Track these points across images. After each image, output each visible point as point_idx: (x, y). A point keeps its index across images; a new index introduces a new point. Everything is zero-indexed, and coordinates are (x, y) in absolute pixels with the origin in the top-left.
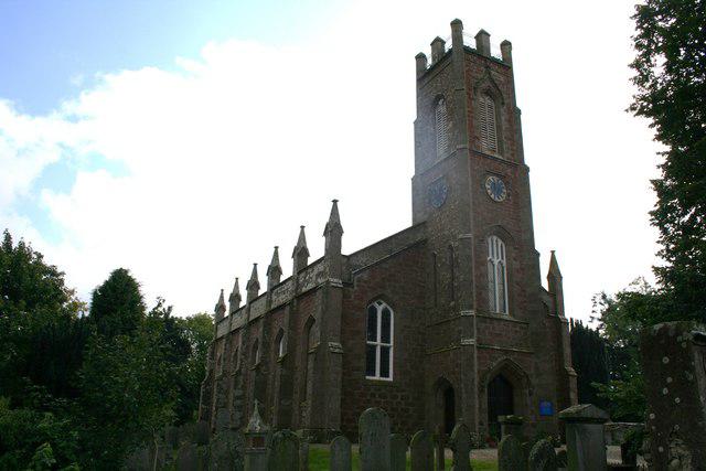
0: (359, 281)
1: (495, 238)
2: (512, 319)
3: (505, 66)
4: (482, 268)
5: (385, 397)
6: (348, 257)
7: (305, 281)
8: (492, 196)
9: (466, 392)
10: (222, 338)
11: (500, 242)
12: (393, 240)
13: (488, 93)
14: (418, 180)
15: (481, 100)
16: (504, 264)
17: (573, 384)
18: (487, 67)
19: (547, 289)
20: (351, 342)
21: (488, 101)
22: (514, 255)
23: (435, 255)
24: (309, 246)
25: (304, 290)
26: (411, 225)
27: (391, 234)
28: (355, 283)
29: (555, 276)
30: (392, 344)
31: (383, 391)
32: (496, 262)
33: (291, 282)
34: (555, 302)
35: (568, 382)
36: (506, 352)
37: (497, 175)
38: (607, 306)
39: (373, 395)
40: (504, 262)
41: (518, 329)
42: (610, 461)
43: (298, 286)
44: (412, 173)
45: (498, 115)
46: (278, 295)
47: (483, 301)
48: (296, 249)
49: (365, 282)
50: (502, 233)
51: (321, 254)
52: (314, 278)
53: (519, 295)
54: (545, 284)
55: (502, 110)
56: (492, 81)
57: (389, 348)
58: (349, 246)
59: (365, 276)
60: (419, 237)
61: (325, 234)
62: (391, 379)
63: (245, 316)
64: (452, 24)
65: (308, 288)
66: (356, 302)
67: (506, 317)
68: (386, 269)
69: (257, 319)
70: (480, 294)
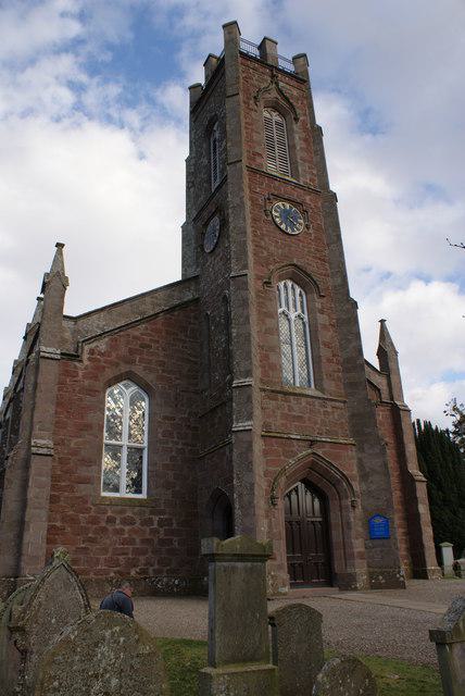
0: (92, 352)
1: (290, 283)
2: (320, 394)
3: (301, 79)
4: (268, 321)
5: (132, 522)
6: (75, 319)
8: (283, 227)
9: (242, 507)
11: (298, 290)
12: (148, 299)
13: (275, 107)
14: (190, 227)
15: (266, 114)
16: (306, 320)
17: (422, 491)
18: (273, 76)
19: (377, 367)
20: (75, 440)
21: (276, 117)
22: (318, 306)
26: (179, 278)
27: (145, 291)
28: (85, 356)
29: (386, 351)
30: (146, 444)
31: (129, 514)
32: (293, 316)
34: (389, 384)
35: (414, 490)
36: (312, 443)
37: (288, 200)
38: (458, 417)
39: (111, 520)
42: (204, 542)
44: (183, 219)
45: (290, 132)
47: (272, 368)
49: (102, 354)
50: (301, 277)
53: (329, 361)
54: (370, 354)
55: (295, 127)
56: (280, 91)
58: (74, 305)
59: (102, 345)
60: (189, 296)
62: (143, 496)
66: (87, 382)
67: (309, 392)
68: (135, 338)
70: (267, 356)
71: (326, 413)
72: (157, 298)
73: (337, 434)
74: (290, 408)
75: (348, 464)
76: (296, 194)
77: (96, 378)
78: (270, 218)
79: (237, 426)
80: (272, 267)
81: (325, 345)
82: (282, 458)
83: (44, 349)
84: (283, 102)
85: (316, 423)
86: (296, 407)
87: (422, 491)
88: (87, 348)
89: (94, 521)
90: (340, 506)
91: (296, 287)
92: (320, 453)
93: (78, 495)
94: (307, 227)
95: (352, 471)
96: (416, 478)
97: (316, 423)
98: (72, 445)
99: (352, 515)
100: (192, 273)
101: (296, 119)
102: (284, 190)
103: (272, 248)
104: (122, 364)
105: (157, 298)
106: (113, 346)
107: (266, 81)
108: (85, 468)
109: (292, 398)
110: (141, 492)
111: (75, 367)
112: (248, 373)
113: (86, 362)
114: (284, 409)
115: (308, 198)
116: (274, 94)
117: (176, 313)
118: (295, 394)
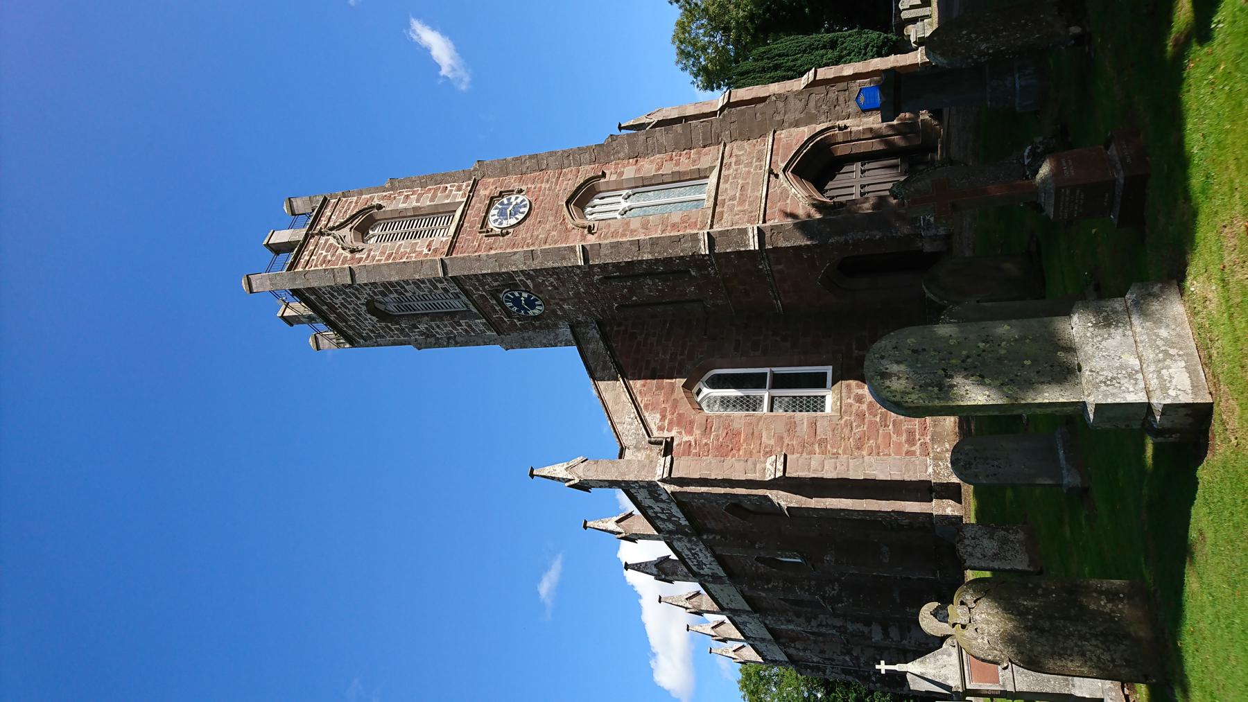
1: (588, 210)
7: (669, 520)
10: (786, 653)
11: (596, 201)
14: (508, 338)
17: (825, 73)
18: (321, 233)
23: (621, 307)
24: (653, 557)
25: (684, 522)
26: (575, 348)
28: (666, 434)
30: (767, 370)
32: (625, 205)
33: (676, 544)
37: (487, 212)
40: (624, 193)
41: (733, 160)
43: (680, 530)
46: (700, 565)
48: (658, 578)
49: (663, 418)
51: (662, 544)
52: (662, 505)
53: (677, 164)
57: (774, 376)
59: (653, 419)
60: (594, 333)
61: (671, 582)
62: (829, 370)
63: (744, 618)
64: (640, 596)
65: (680, 515)
69: (748, 600)
71: (738, 163)
72: (596, 366)
73: (761, 152)
74: (733, 198)
75: (796, 137)
76: (478, 205)
77: (692, 423)
78: (511, 230)
79: (753, 245)
80: (570, 226)
81: (659, 169)
82: (788, 201)
83: (659, 472)
84: (356, 222)
85: (749, 172)
86: (731, 193)
87: (825, 73)
88: (656, 434)
89: (861, 416)
90: (844, 142)
91: (591, 203)
92: (783, 165)
93: (830, 434)
94: (520, 191)
95: (805, 132)
96: (811, 79)
97: (749, 172)
98: (772, 442)
99: (854, 129)
100: (565, 331)
101: (380, 207)
102: (474, 216)
103: (548, 227)
104: (675, 396)
105: (596, 366)
106: (652, 407)
107: (327, 241)
108: (798, 429)
109: (719, 198)
110: (825, 374)
111: (679, 445)
112: (695, 238)
113: (673, 433)
114: (734, 205)
115: (482, 192)
116: (345, 231)
117: (614, 345)
118: (715, 205)
